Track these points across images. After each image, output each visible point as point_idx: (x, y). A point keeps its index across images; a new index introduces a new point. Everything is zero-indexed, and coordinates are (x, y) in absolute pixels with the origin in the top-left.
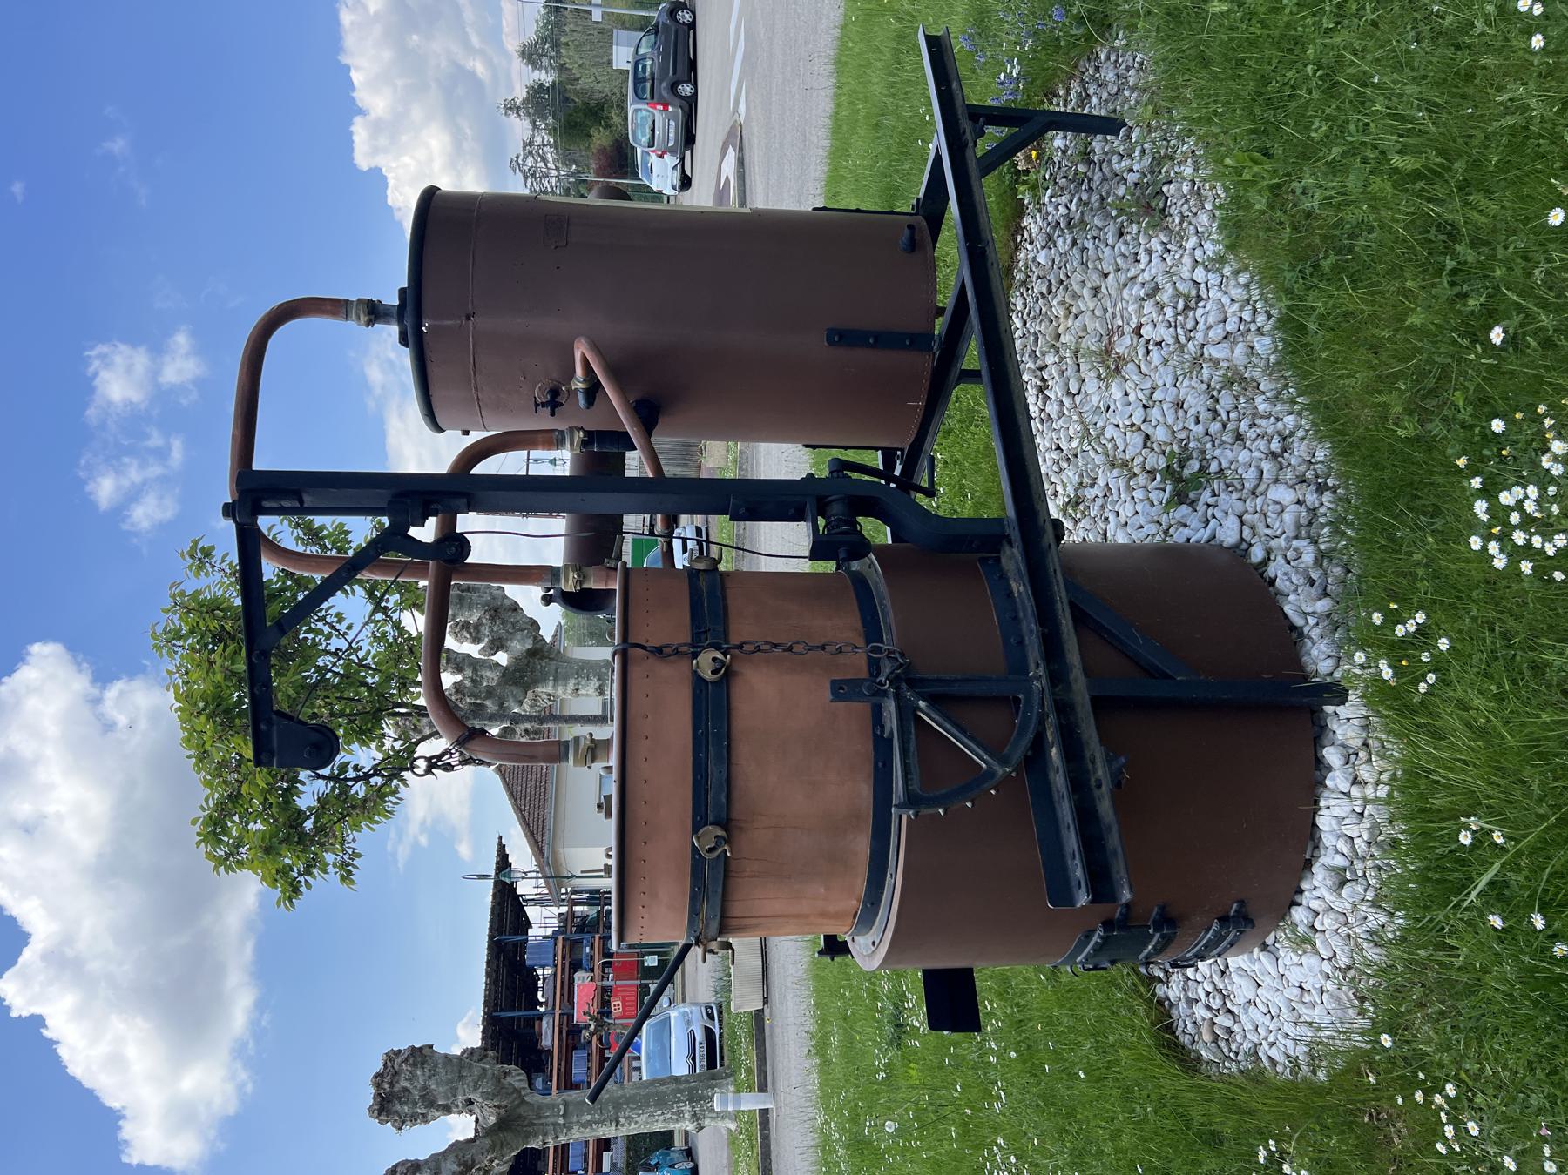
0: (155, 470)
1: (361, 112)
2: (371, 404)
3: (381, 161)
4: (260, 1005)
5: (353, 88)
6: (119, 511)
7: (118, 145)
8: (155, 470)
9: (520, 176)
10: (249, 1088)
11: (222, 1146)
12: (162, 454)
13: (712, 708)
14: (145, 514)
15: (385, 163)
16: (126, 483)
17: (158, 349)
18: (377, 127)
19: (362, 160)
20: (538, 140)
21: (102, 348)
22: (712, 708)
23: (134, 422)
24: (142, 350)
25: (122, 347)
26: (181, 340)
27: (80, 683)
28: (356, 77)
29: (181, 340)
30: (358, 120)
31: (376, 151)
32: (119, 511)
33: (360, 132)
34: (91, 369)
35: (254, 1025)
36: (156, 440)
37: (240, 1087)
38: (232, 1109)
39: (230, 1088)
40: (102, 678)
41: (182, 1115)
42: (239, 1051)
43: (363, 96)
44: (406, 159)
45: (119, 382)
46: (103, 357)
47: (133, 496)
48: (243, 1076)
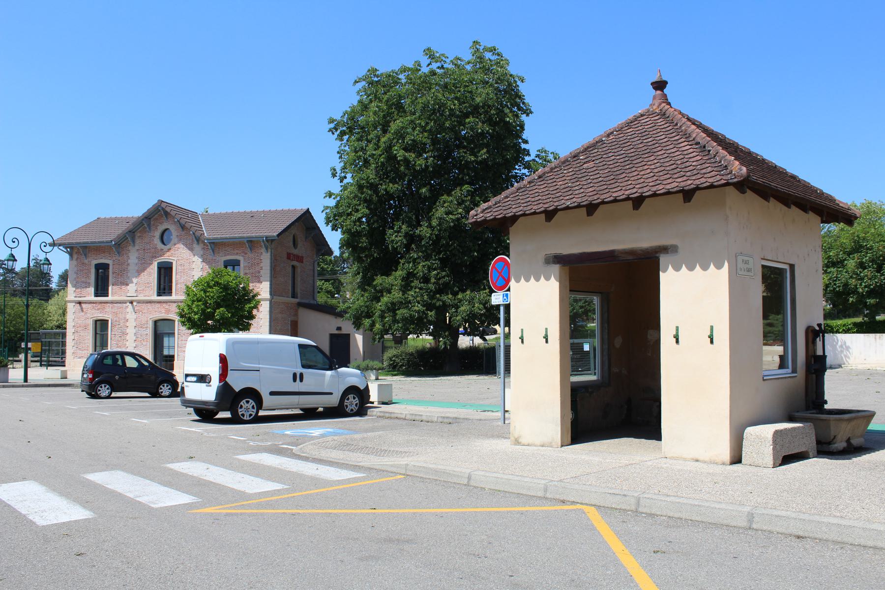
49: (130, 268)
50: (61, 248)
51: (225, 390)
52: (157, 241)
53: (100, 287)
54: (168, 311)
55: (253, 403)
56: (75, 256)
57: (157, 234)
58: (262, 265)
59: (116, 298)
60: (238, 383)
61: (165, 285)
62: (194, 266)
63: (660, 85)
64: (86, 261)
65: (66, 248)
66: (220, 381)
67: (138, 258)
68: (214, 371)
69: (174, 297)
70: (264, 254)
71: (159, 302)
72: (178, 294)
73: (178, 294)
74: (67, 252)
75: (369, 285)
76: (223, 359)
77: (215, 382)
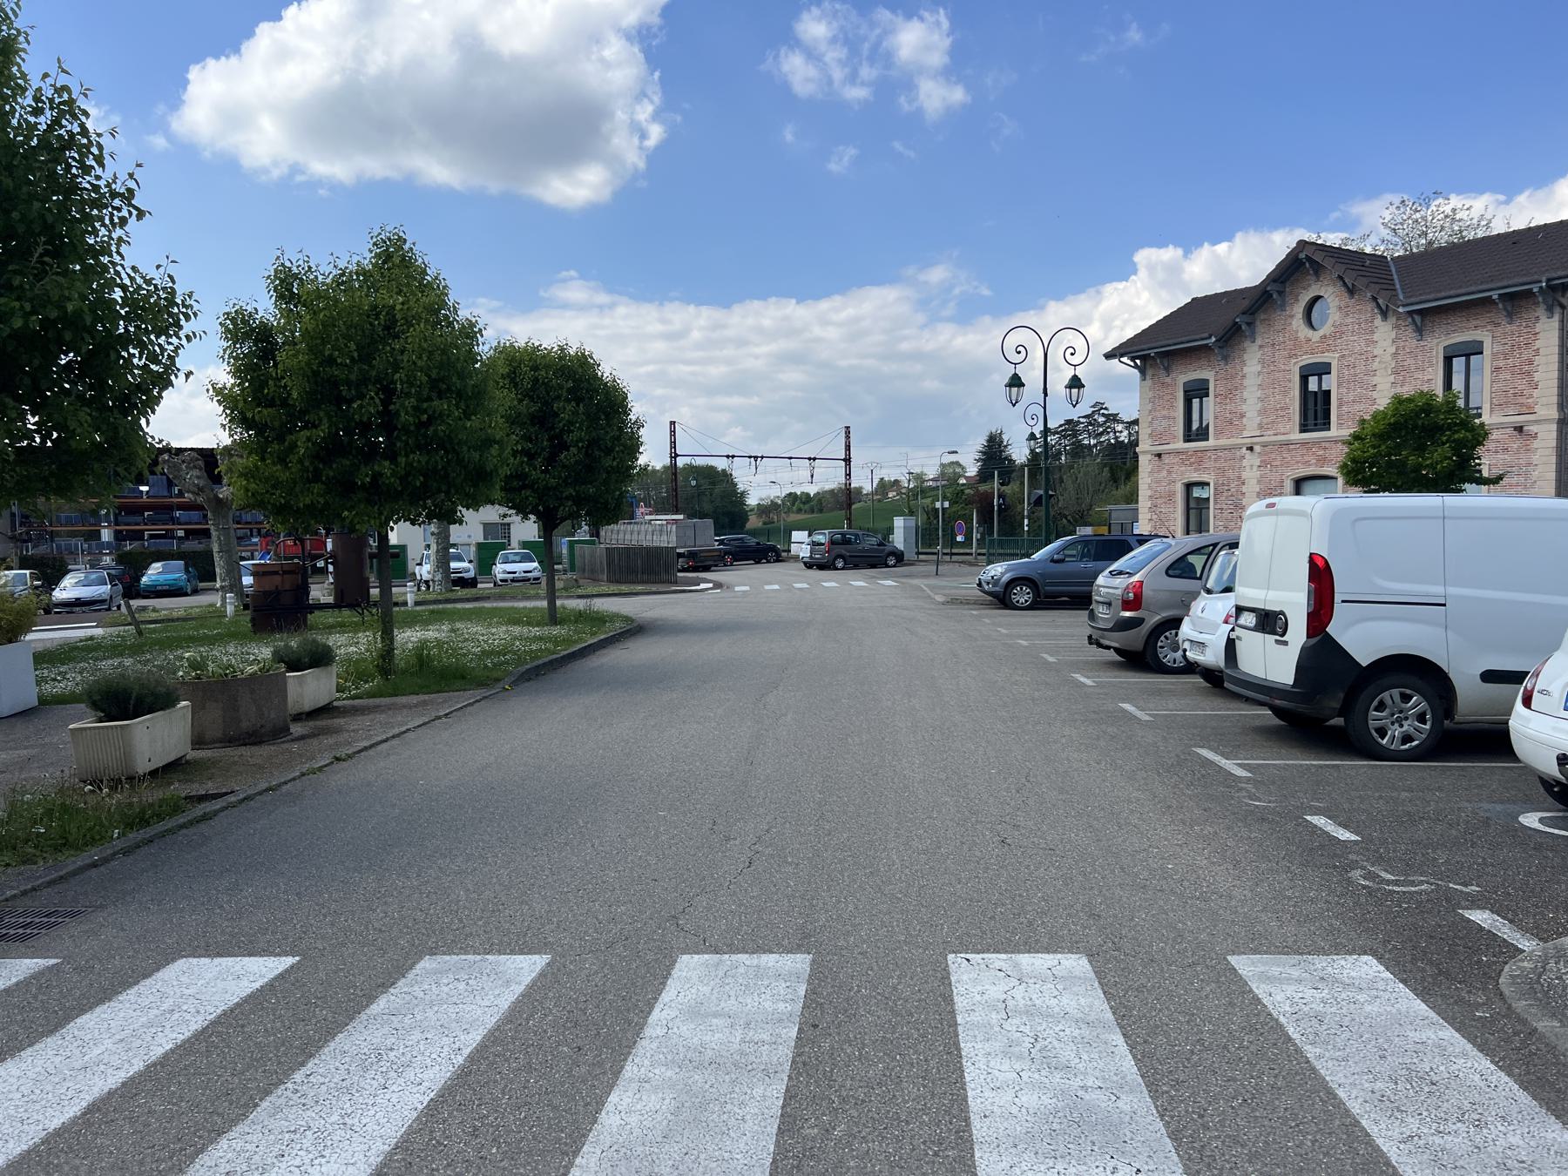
0: (838, 74)
1: (1187, 253)
2: (910, 271)
3: (1142, 273)
4: (335, 187)
5: (1214, 243)
6: (794, 43)
7: (1134, 35)
8: (838, 74)
9: (1089, 411)
10: (264, 178)
11: (207, 154)
12: (853, 78)
13: (276, 573)
14: (796, 68)
15: (1140, 280)
16: (823, 47)
17: (950, 73)
18: (1174, 270)
19: (1143, 256)
20: (1119, 427)
21: (945, 24)
22: (276, 573)
23: (882, 56)
24: (946, 59)
25: (948, 42)
26: (958, 95)
27: (632, 19)
28: (1222, 248)
29: (958, 95)
30: (1180, 252)
31: (1151, 268)
32: (794, 43)
33: (1170, 254)
34: (926, 15)
35: (315, 183)
36: (866, 72)
37: (266, 171)
38: (247, 162)
39: (265, 161)
40: (641, 36)
41: (235, 117)
42: (295, 169)
43: (1206, 251)
44: (1145, 295)
45: (916, 40)
46: (938, 24)
47: (811, 55)
48: (276, 173)
49: (1246, 382)
50: (1125, 359)
51: (1322, 655)
52: (1298, 322)
53: (1311, 414)
54: (1322, 461)
55: (1396, 692)
56: (1149, 372)
57: (1299, 309)
58: (1538, 344)
59: (1223, 442)
60: (1363, 638)
61: (1316, 410)
62: (1376, 365)
63: (139, 165)
64: (1168, 380)
65: (1133, 359)
66: (1311, 632)
67: (1262, 362)
68: (1295, 602)
69: (1334, 432)
70: (1543, 319)
71: (1304, 444)
72: (1341, 428)
73: (1341, 428)
74: (1136, 366)
75: (610, 509)
76: (1320, 575)
77: (1298, 633)
